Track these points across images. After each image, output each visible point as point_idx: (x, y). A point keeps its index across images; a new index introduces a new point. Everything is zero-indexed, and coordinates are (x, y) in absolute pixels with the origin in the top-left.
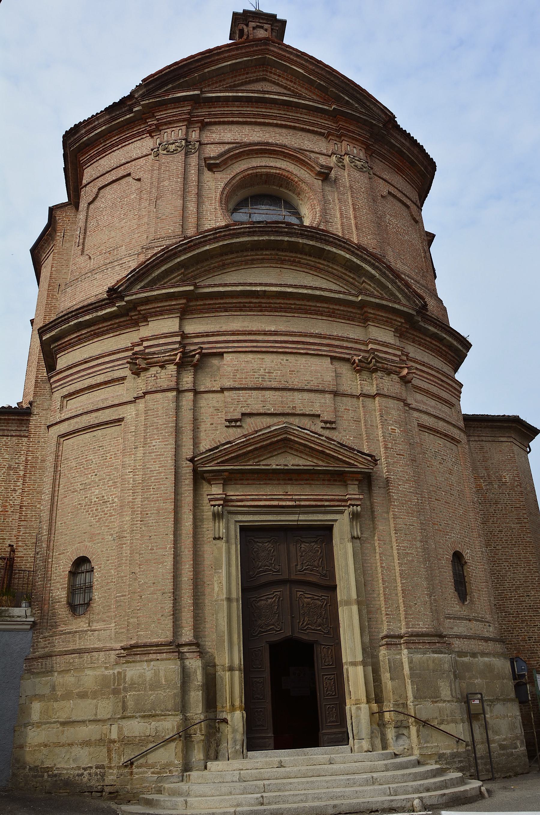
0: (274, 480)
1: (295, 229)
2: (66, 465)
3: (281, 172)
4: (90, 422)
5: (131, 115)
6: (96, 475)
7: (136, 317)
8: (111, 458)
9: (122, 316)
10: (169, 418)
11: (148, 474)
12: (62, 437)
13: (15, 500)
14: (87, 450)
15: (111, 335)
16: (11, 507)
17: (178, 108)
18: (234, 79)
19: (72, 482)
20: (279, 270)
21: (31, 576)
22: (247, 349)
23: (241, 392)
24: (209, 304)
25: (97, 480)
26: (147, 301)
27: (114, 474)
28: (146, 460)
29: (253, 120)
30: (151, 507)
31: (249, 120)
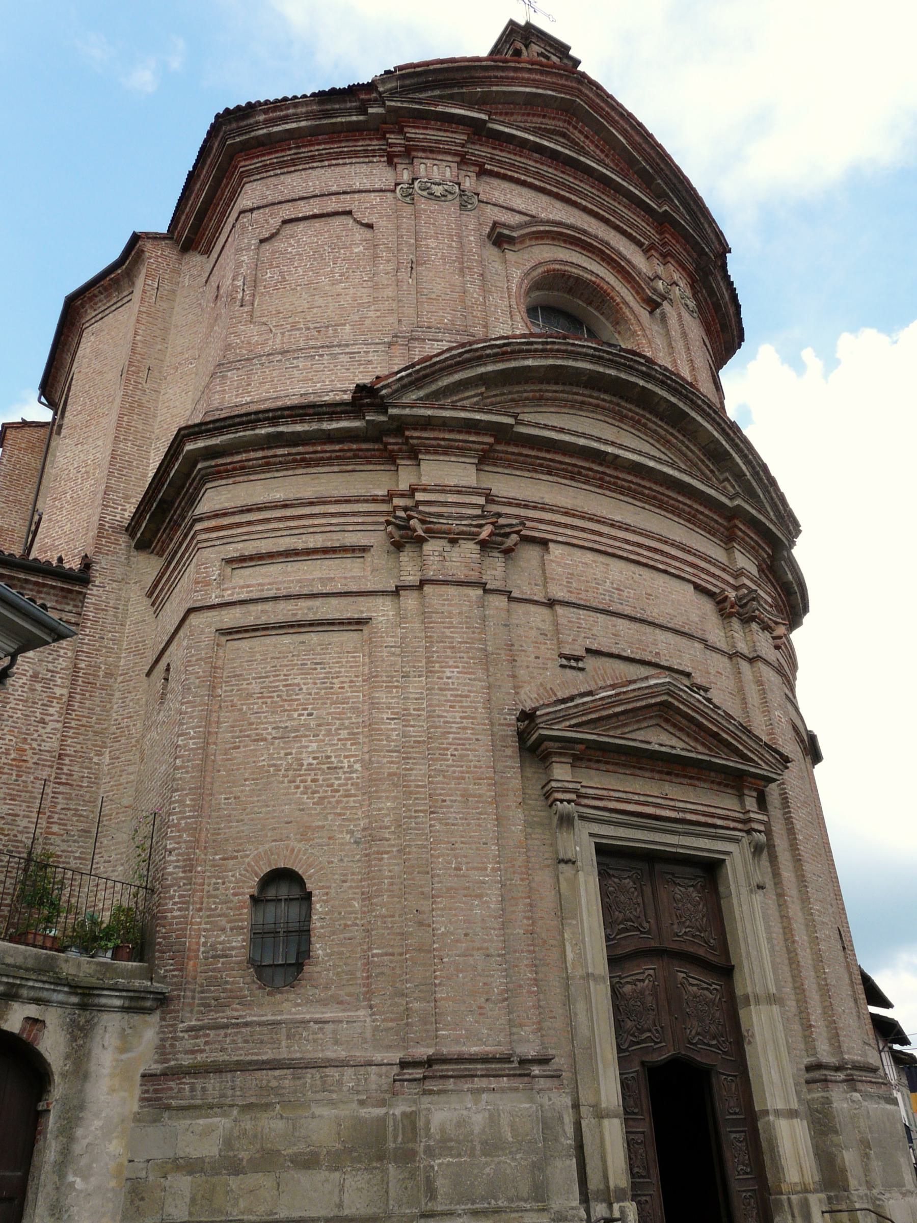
0: (646, 770)
1: (656, 370)
2: (235, 688)
3: (598, 281)
4: (295, 615)
5: (361, 118)
6: (310, 714)
7: (396, 447)
8: (343, 688)
9: (366, 440)
10: (474, 633)
11: (439, 727)
12: (223, 634)
13: (43, 741)
14: (287, 666)
15: (336, 469)
16: (34, 754)
17: (446, 131)
18: (526, 118)
19: (253, 720)
20: (616, 429)
21: (74, 896)
22: (586, 544)
23: (581, 612)
24: (527, 456)
25: (313, 724)
26: (427, 423)
27: (351, 718)
28: (435, 702)
29: (555, 190)
30: (450, 789)
31: (548, 187)
